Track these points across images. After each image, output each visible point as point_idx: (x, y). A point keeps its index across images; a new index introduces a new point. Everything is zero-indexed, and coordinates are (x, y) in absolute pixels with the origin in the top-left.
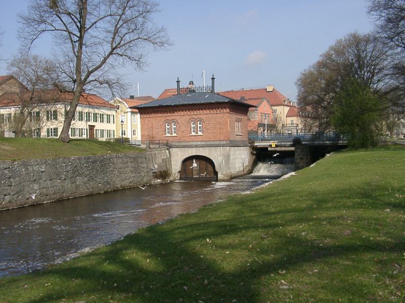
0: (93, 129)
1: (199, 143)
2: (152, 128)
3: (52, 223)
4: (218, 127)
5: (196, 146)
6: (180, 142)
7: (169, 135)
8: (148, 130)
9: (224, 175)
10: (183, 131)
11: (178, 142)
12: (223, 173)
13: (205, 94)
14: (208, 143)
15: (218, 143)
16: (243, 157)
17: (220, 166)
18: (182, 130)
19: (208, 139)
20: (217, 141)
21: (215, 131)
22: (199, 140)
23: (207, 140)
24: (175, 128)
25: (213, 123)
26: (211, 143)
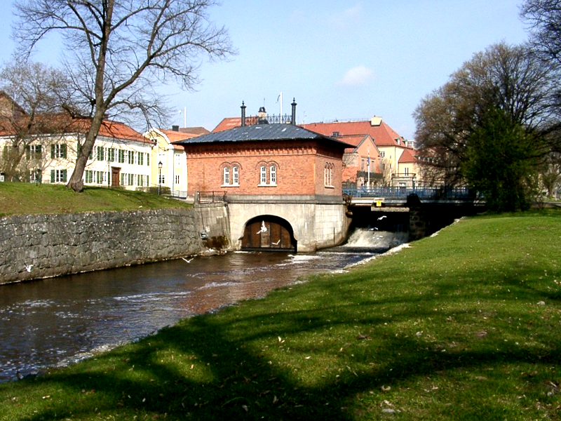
0: (118, 173)
1: (271, 198)
2: (204, 173)
3: (54, 308)
4: (299, 175)
5: (267, 202)
6: (244, 195)
7: (228, 185)
8: (197, 177)
9: (306, 245)
10: (248, 180)
11: (240, 195)
12: (305, 243)
13: (281, 126)
14: (284, 198)
15: (298, 198)
16: (334, 219)
17: (300, 231)
18: (247, 178)
19: (284, 193)
20: (297, 195)
21: (295, 181)
22: (271, 193)
23: (282, 193)
24: (236, 176)
25: (292, 170)
26: (289, 198)
